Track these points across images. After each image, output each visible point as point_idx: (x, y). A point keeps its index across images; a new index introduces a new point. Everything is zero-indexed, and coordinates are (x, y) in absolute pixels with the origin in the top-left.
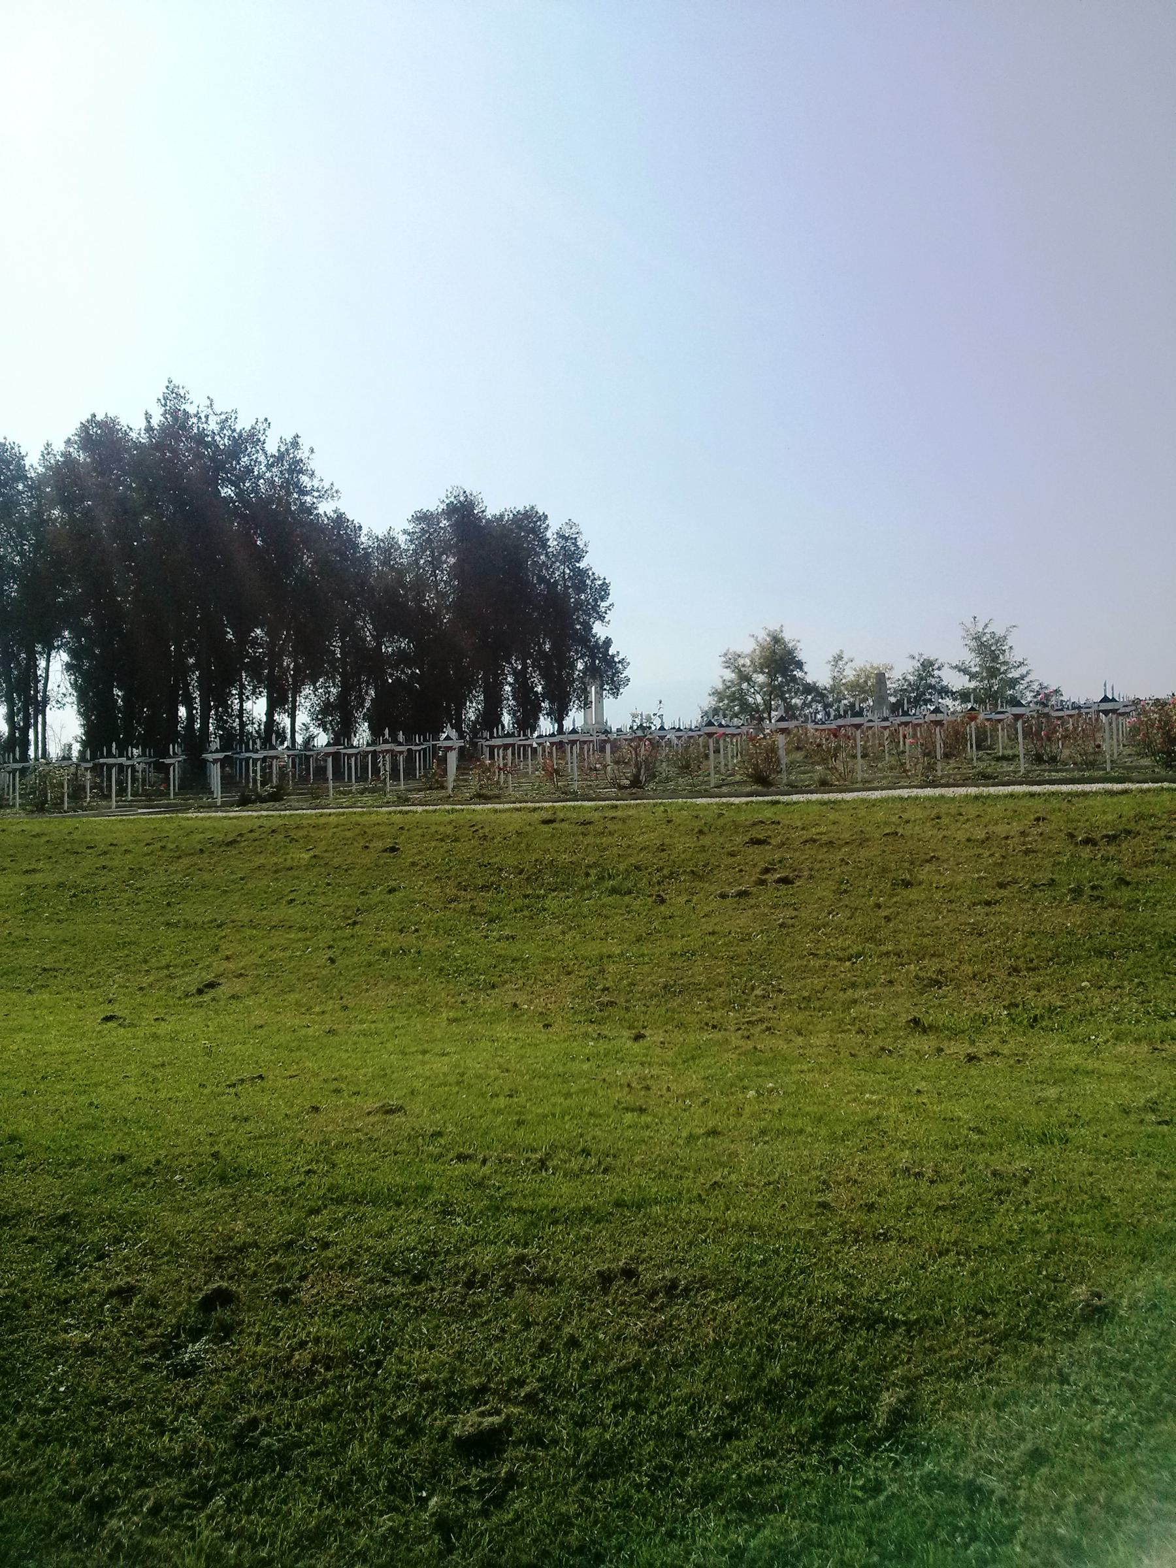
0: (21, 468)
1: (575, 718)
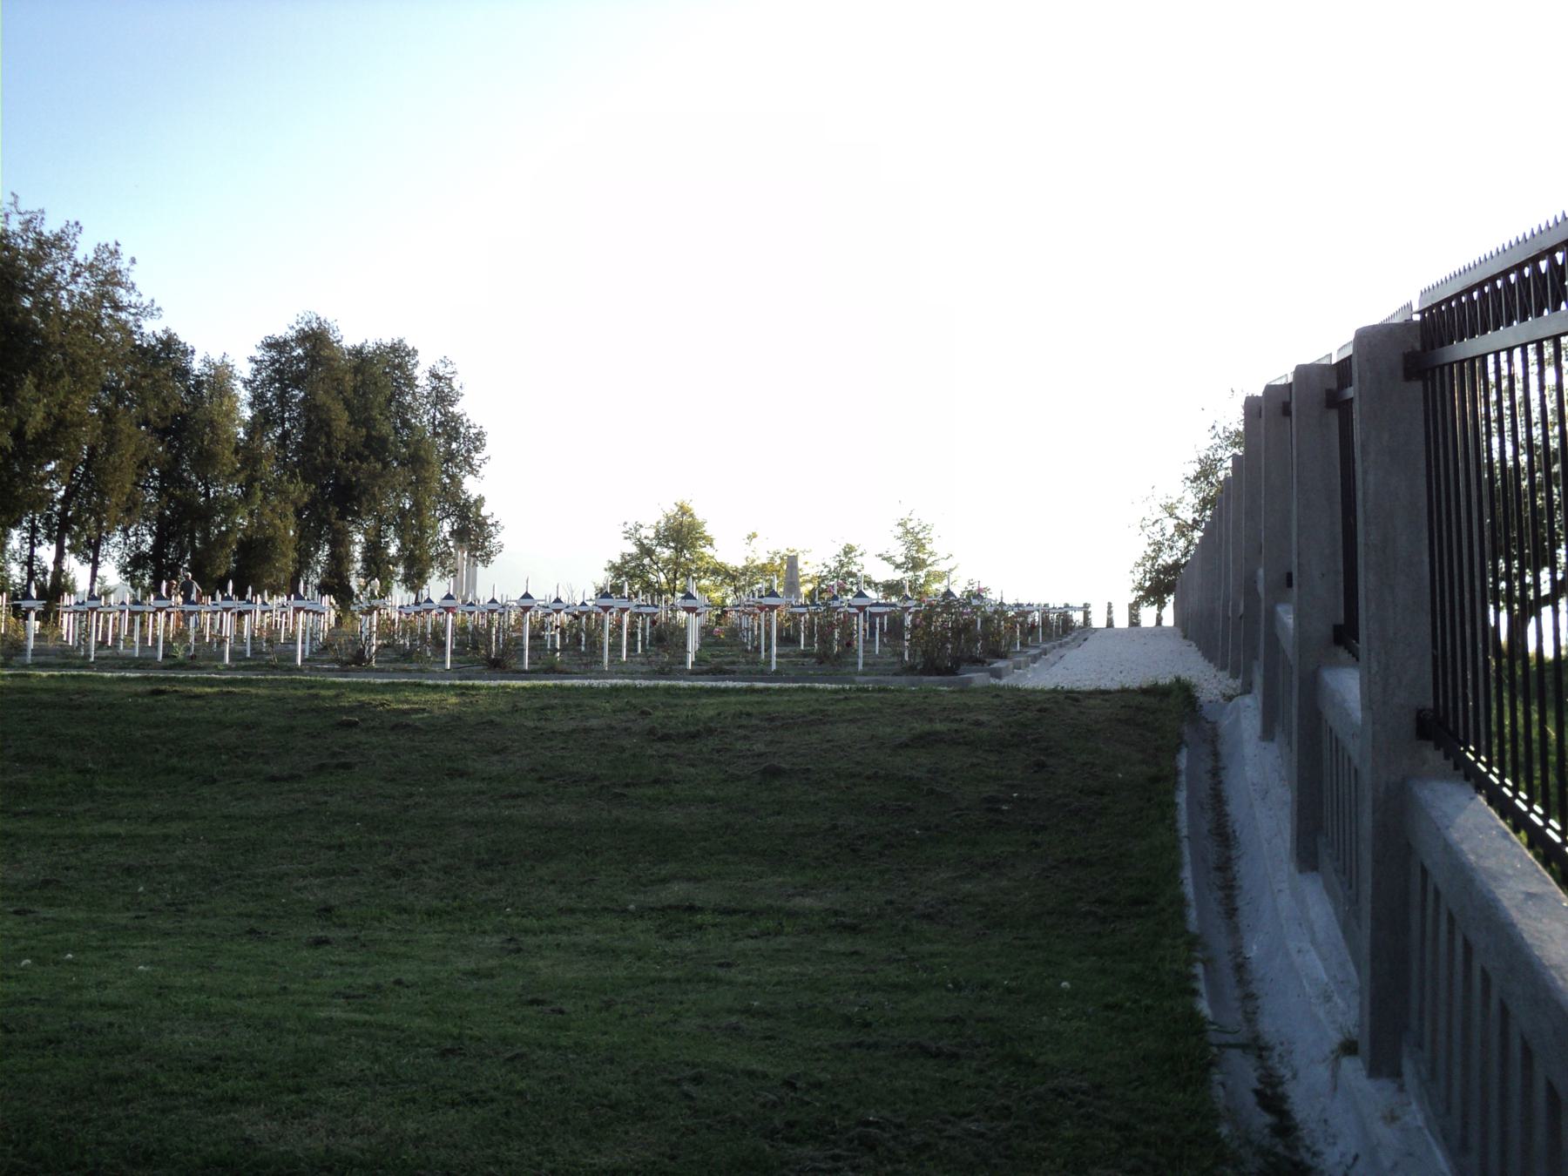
1: (437, 587)
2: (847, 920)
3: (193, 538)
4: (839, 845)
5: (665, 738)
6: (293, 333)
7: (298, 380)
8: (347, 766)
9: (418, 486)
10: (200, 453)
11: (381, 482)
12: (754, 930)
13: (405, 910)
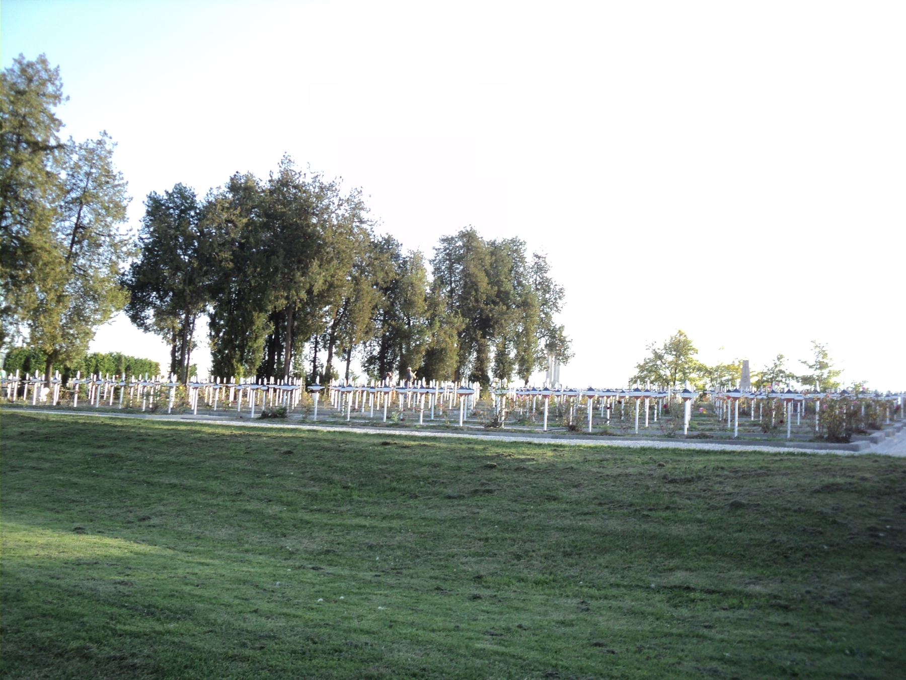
0: (193, 202)
1: (538, 378)
2: (782, 602)
3: (401, 348)
4: (778, 553)
5: (673, 481)
7: (459, 259)
8: (489, 491)
9: (527, 319)
10: (405, 301)
11: (506, 317)
12: (725, 604)
13: (523, 580)
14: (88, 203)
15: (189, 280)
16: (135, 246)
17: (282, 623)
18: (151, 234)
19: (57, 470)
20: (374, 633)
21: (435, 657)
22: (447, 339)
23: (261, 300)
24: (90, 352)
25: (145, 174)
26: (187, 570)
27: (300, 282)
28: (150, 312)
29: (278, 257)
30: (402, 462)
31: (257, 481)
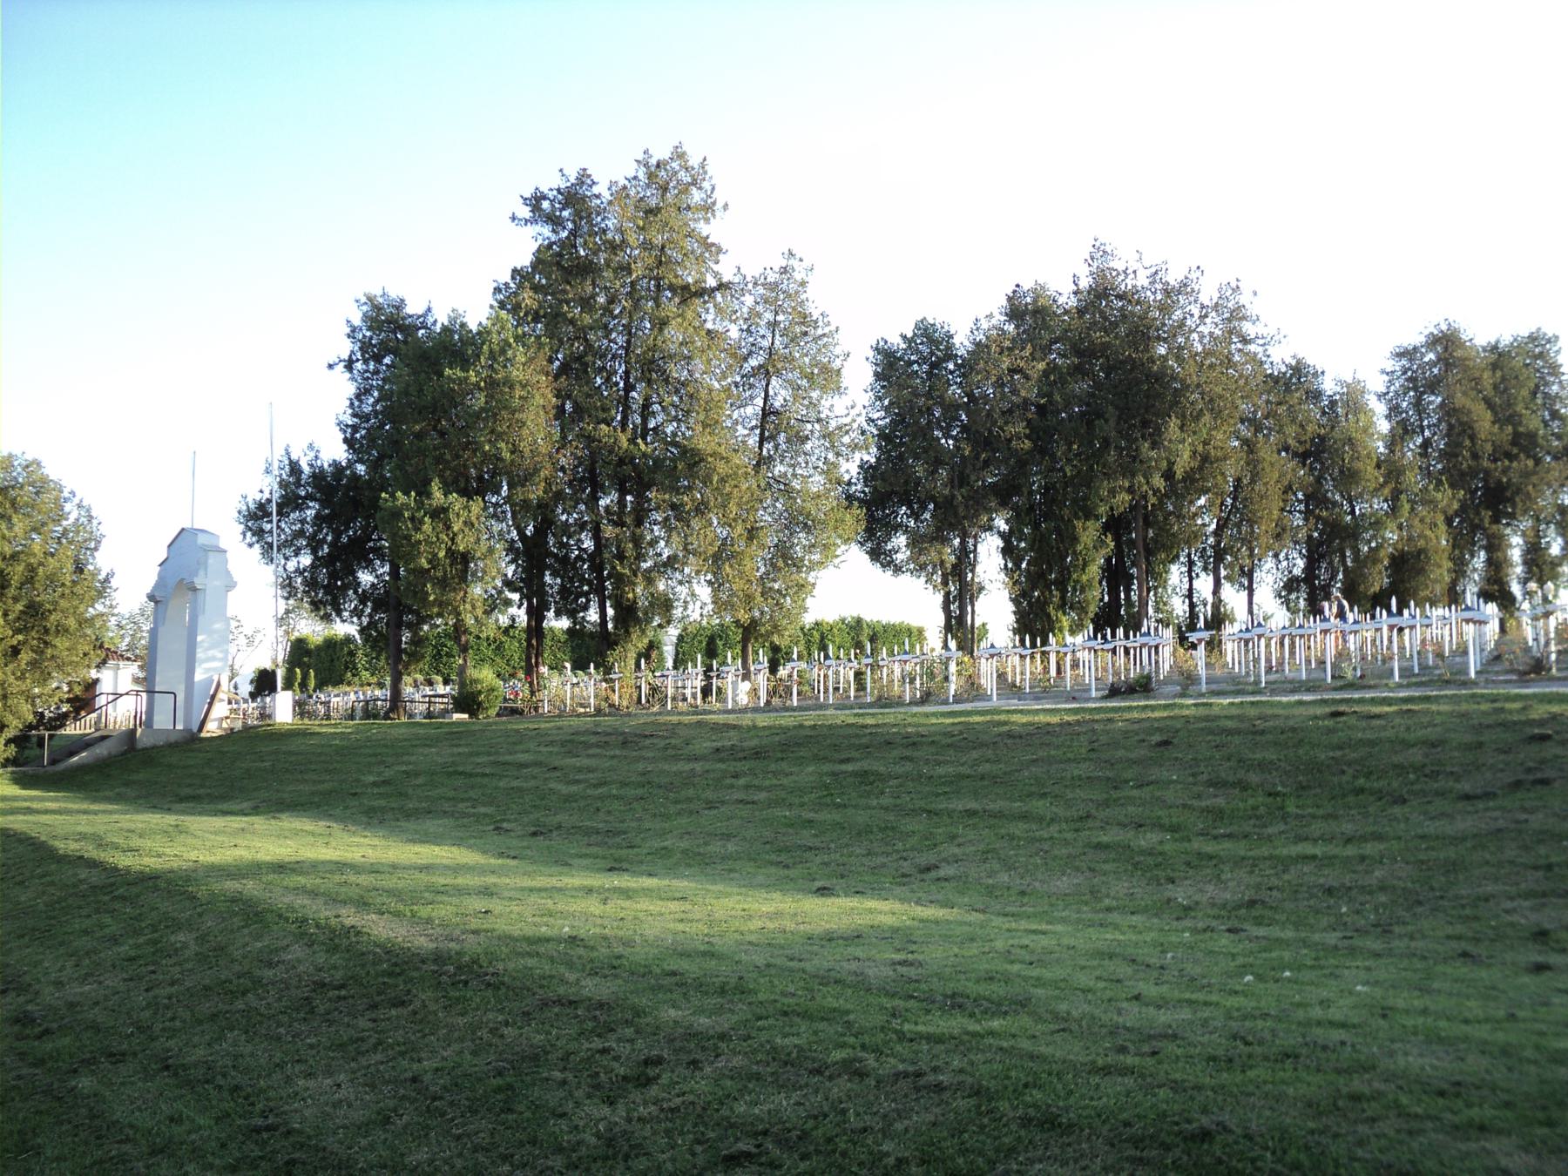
0: (950, 347)
3: (1343, 557)
6: (1423, 339)
7: (1433, 386)
8: (1544, 782)
10: (1342, 472)
11: (1534, 479)
14: (778, 373)
15: (960, 479)
16: (863, 433)
17: (1185, 1014)
18: (887, 409)
19: (778, 803)
20: (1354, 1026)
21: (1475, 1064)
22: (1428, 533)
23: (1085, 498)
24: (808, 619)
25: (862, 320)
26: (1011, 942)
27: (1150, 459)
28: (900, 540)
29: (1106, 421)
30: (1371, 743)
31: (1115, 794)
